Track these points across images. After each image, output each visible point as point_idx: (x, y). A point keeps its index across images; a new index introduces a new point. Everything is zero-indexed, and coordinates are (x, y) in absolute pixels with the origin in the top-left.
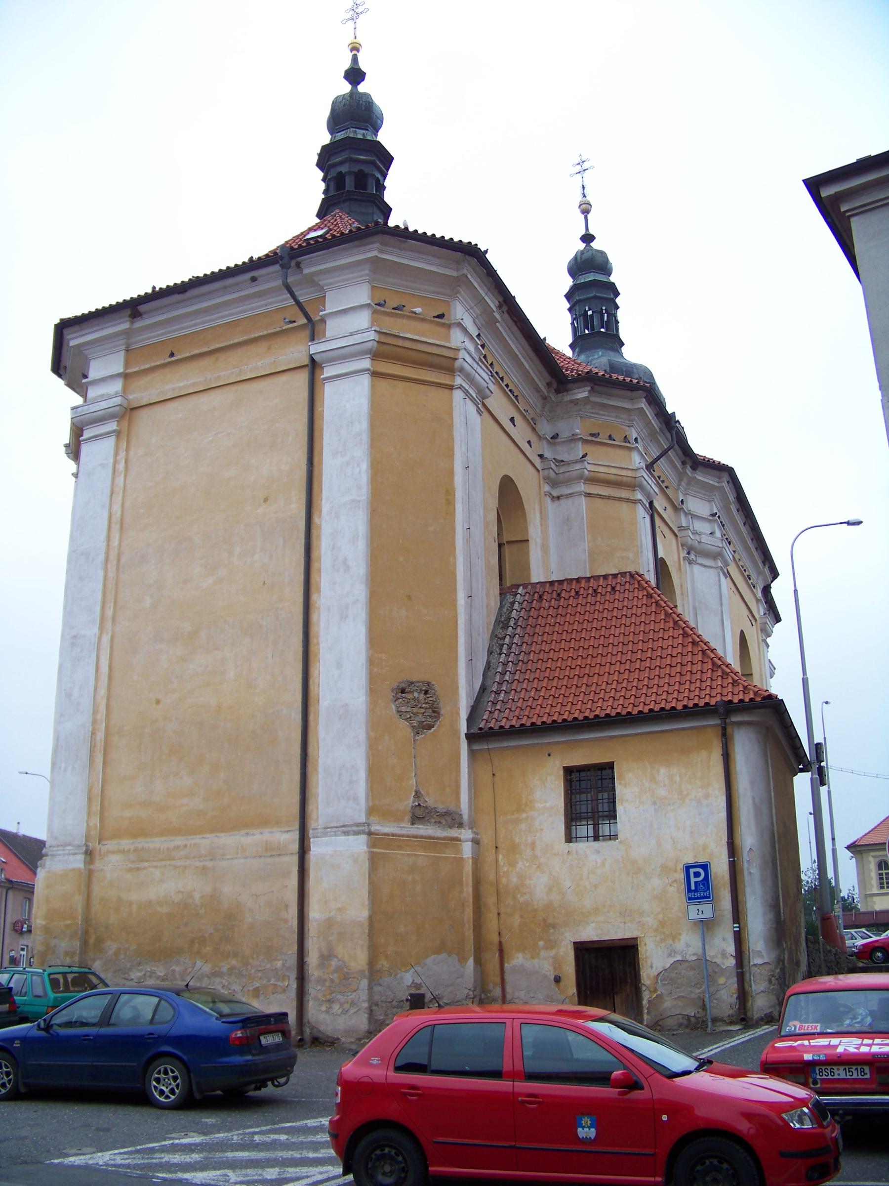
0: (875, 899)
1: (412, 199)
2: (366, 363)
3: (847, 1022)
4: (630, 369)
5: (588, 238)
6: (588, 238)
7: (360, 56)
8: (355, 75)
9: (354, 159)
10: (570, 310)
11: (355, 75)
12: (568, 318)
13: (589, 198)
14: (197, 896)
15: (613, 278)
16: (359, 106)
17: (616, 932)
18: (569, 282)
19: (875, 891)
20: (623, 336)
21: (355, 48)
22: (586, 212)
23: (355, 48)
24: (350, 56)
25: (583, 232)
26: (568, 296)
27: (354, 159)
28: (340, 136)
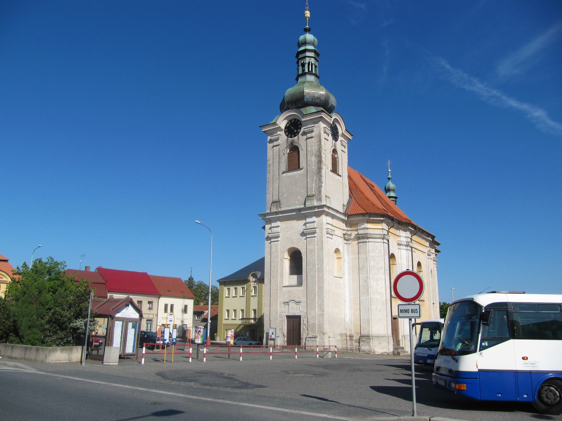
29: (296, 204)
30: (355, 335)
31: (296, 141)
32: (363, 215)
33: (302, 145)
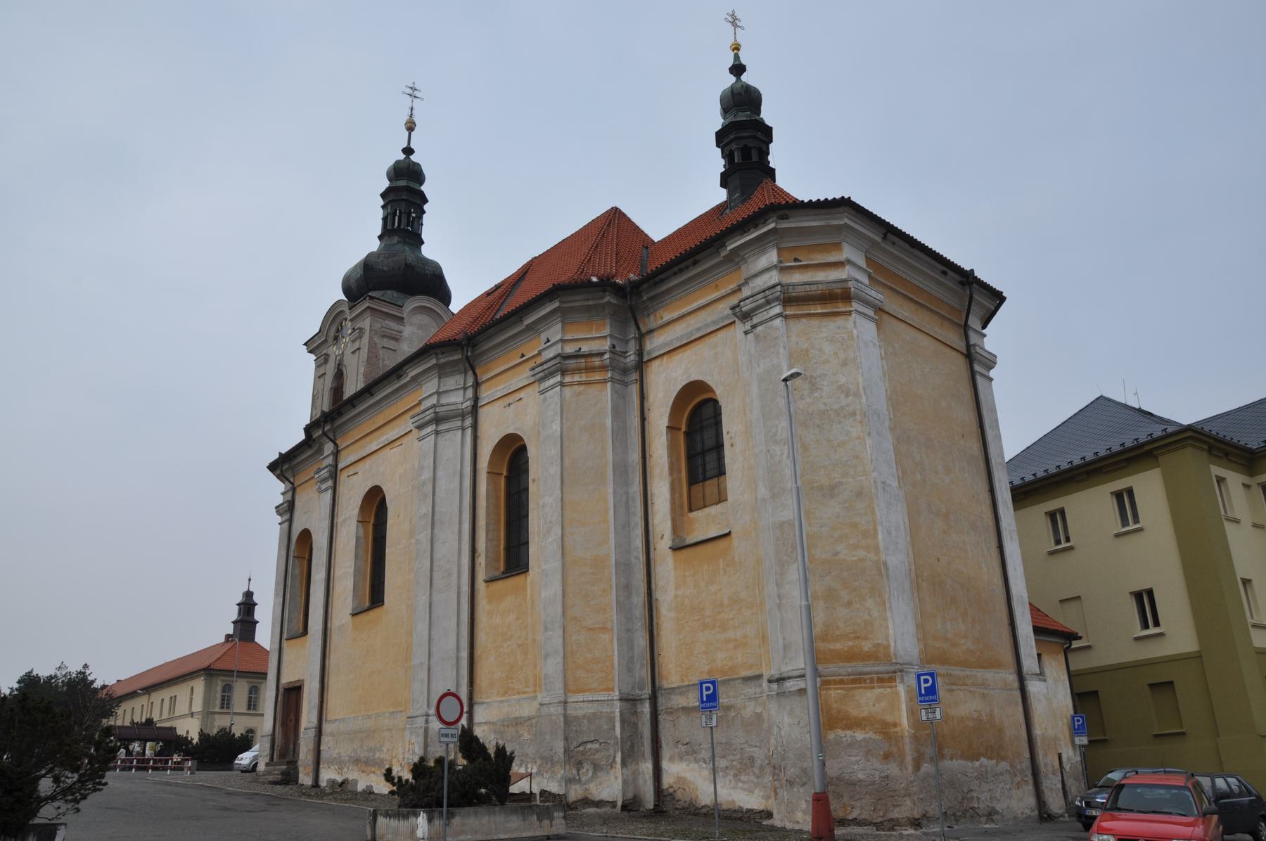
0: (216, 716)
1: (798, 172)
2: (777, 309)
3: (69, 781)
4: (427, 262)
5: (408, 151)
6: (408, 151)
7: (740, 54)
8: (738, 69)
9: (744, 136)
10: (383, 207)
11: (738, 69)
13: (416, 119)
14: (1028, 812)
15: (423, 188)
16: (739, 94)
17: (414, 753)
18: (386, 184)
19: (217, 710)
20: (425, 236)
21: (736, 48)
23: (736, 48)
24: (732, 55)
25: (405, 145)
26: (383, 195)
27: (744, 136)
28: (731, 119)
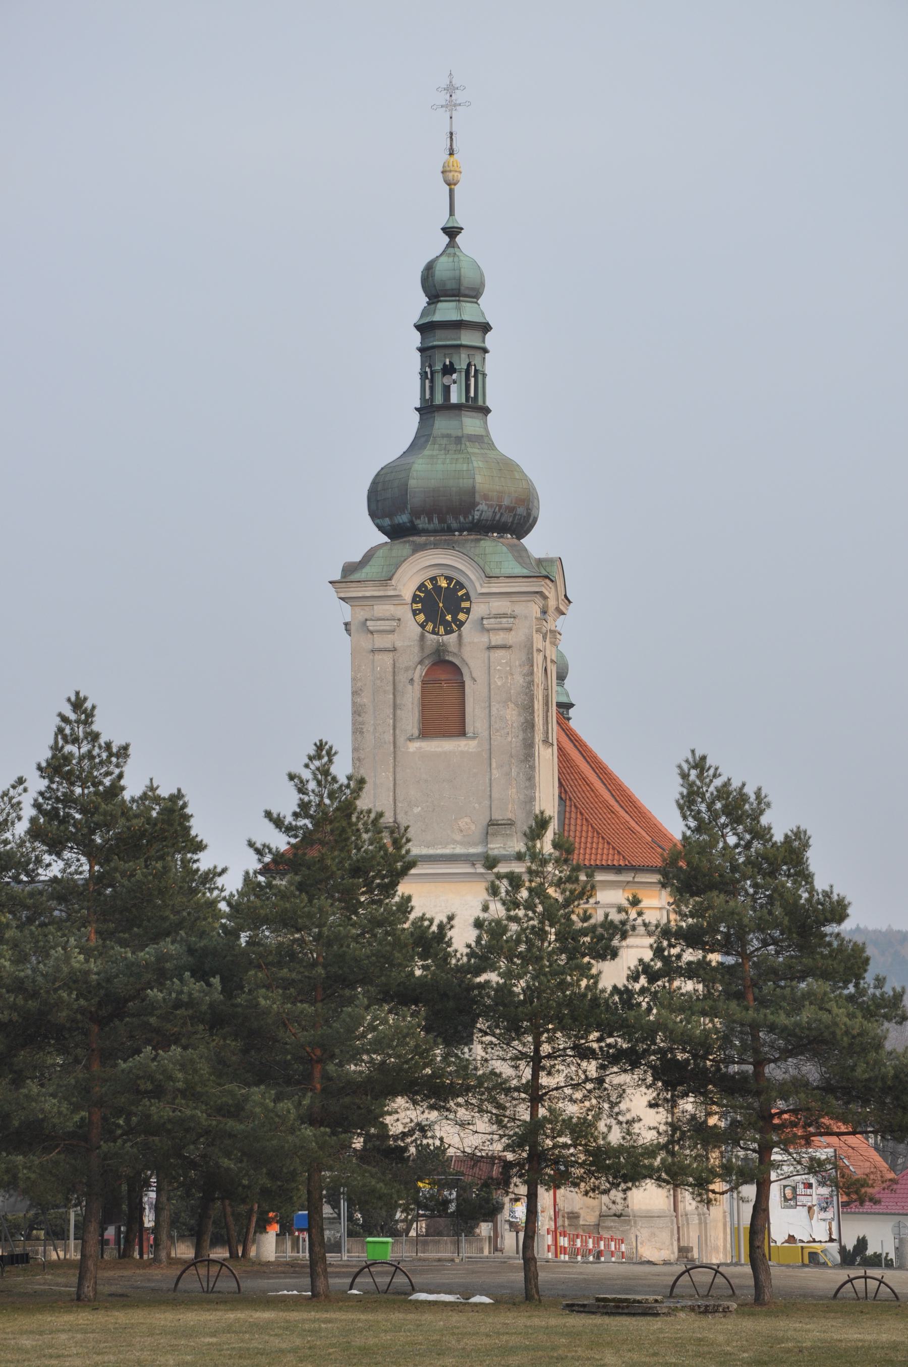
12: (416, 358)
22: (451, 184)
29: (455, 842)
30: (582, 1213)
31: (453, 648)
32: (618, 870)
33: (472, 663)
